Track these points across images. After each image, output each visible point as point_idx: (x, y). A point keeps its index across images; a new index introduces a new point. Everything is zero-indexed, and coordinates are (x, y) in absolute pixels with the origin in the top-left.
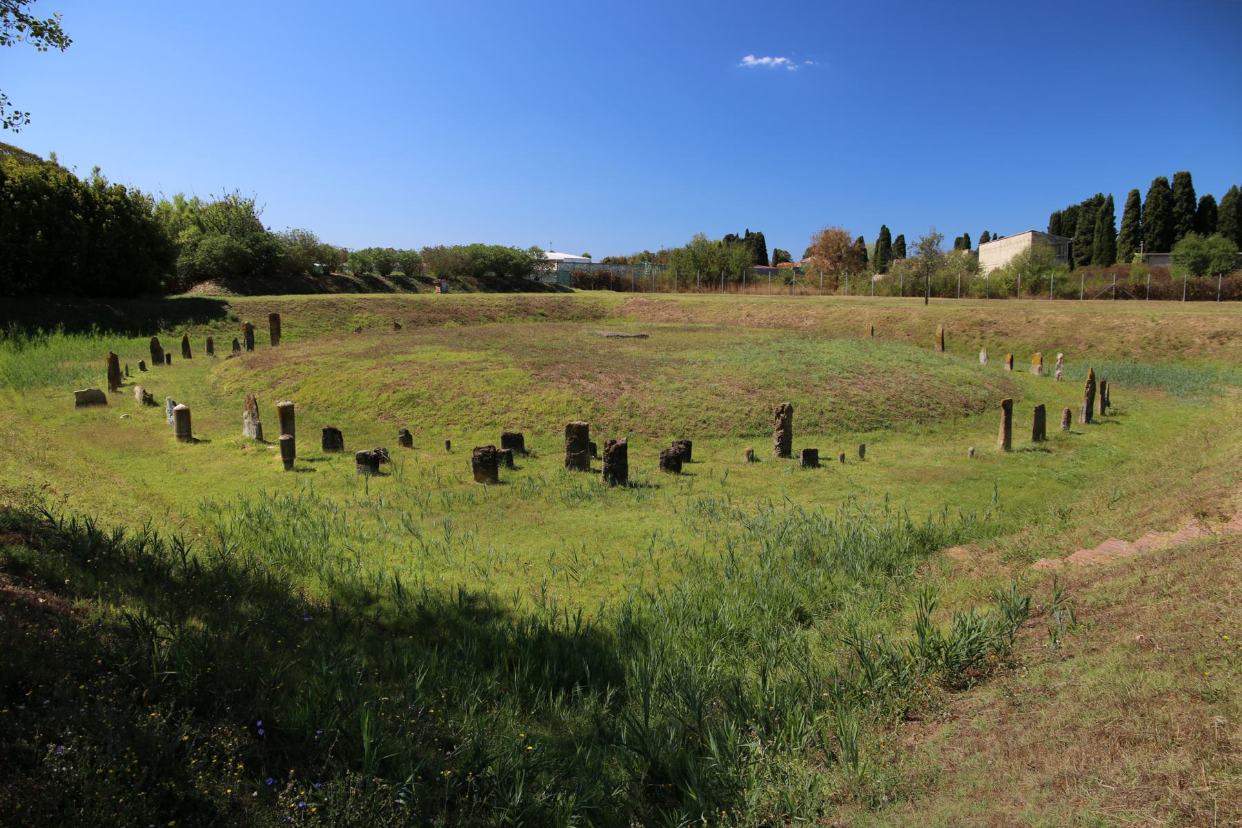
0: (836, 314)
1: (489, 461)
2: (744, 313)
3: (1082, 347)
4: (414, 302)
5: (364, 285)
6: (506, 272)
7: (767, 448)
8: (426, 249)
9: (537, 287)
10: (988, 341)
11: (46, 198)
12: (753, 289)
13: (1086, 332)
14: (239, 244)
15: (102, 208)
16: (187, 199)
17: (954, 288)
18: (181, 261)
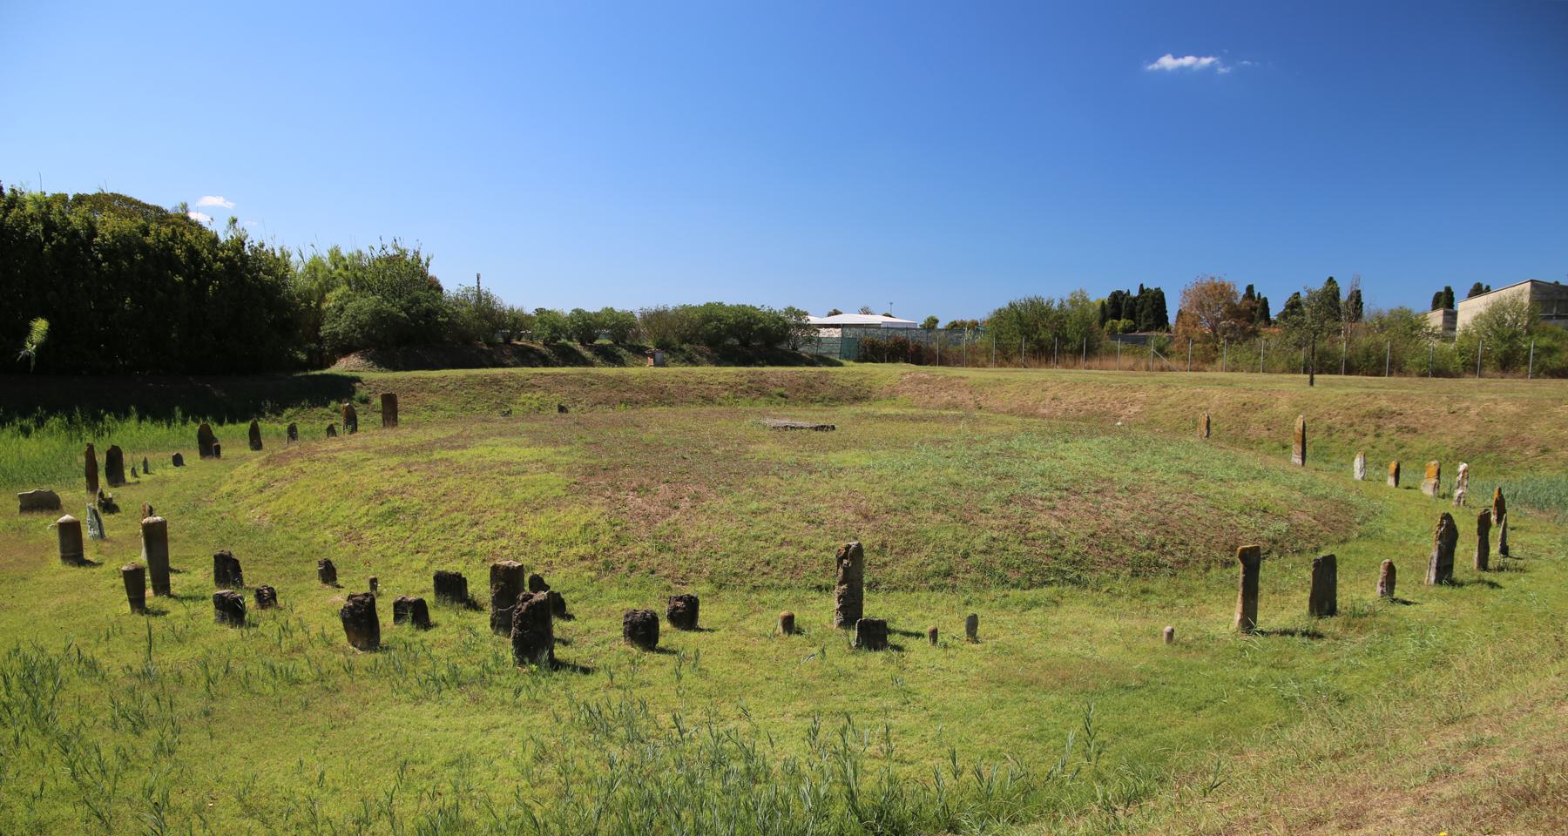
0: (1174, 398)
1: (361, 616)
2: (1050, 394)
3: (1529, 452)
4: (608, 378)
5: (553, 357)
6: (751, 340)
7: (823, 612)
8: (579, 312)
9: (794, 359)
10: (1385, 439)
11: (139, 257)
12: (1096, 363)
13: (1541, 429)
14: (391, 307)
15: (210, 267)
16: (344, 253)
17: (1381, 362)
18: (325, 330)
